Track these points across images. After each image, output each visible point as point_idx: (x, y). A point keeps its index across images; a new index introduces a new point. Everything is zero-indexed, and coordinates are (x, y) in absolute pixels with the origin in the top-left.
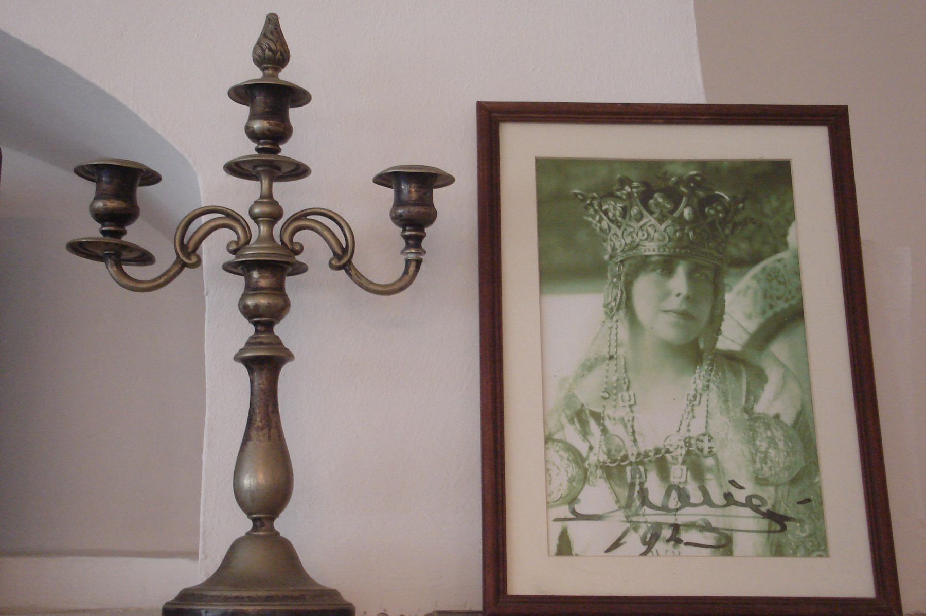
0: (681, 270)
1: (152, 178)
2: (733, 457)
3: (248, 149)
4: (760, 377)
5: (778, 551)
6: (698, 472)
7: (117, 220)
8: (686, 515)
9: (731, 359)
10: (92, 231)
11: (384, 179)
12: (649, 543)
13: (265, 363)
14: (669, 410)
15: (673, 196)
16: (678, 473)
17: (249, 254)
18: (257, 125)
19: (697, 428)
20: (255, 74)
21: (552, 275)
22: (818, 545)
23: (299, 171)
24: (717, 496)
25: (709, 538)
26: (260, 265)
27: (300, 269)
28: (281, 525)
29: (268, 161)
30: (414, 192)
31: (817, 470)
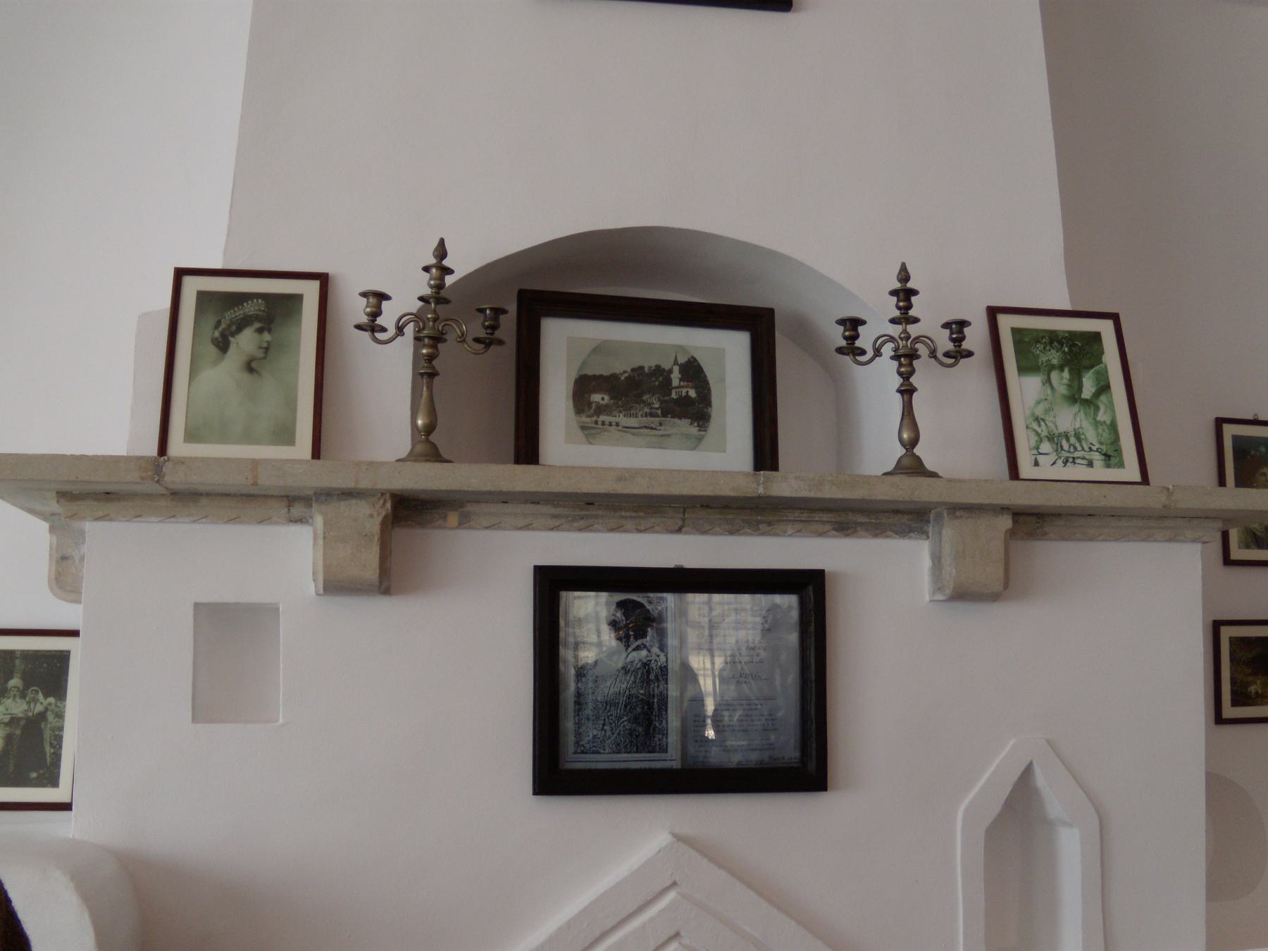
0: (1066, 370)
1: (863, 323)
2: (1091, 435)
3: (897, 313)
4: (1097, 408)
5: (1108, 466)
6: (1079, 440)
8: (1076, 454)
9: (1087, 402)
10: (843, 343)
11: (364, 295)
12: (1065, 463)
14: (1067, 419)
15: (1061, 343)
16: (1073, 440)
17: (901, 352)
18: (901, 304)
19: (1077, 426)
20: (898, 285)
21: (1023, 370)
22: (1121, 465)
23: (916, 320)
24: (1086, 448)
25: (1085, 462)
26: (905, 356)
27: (918, 357)
28: (918, 451)
29: (905, 318)
30: (957, 328)
31: (709, 404)
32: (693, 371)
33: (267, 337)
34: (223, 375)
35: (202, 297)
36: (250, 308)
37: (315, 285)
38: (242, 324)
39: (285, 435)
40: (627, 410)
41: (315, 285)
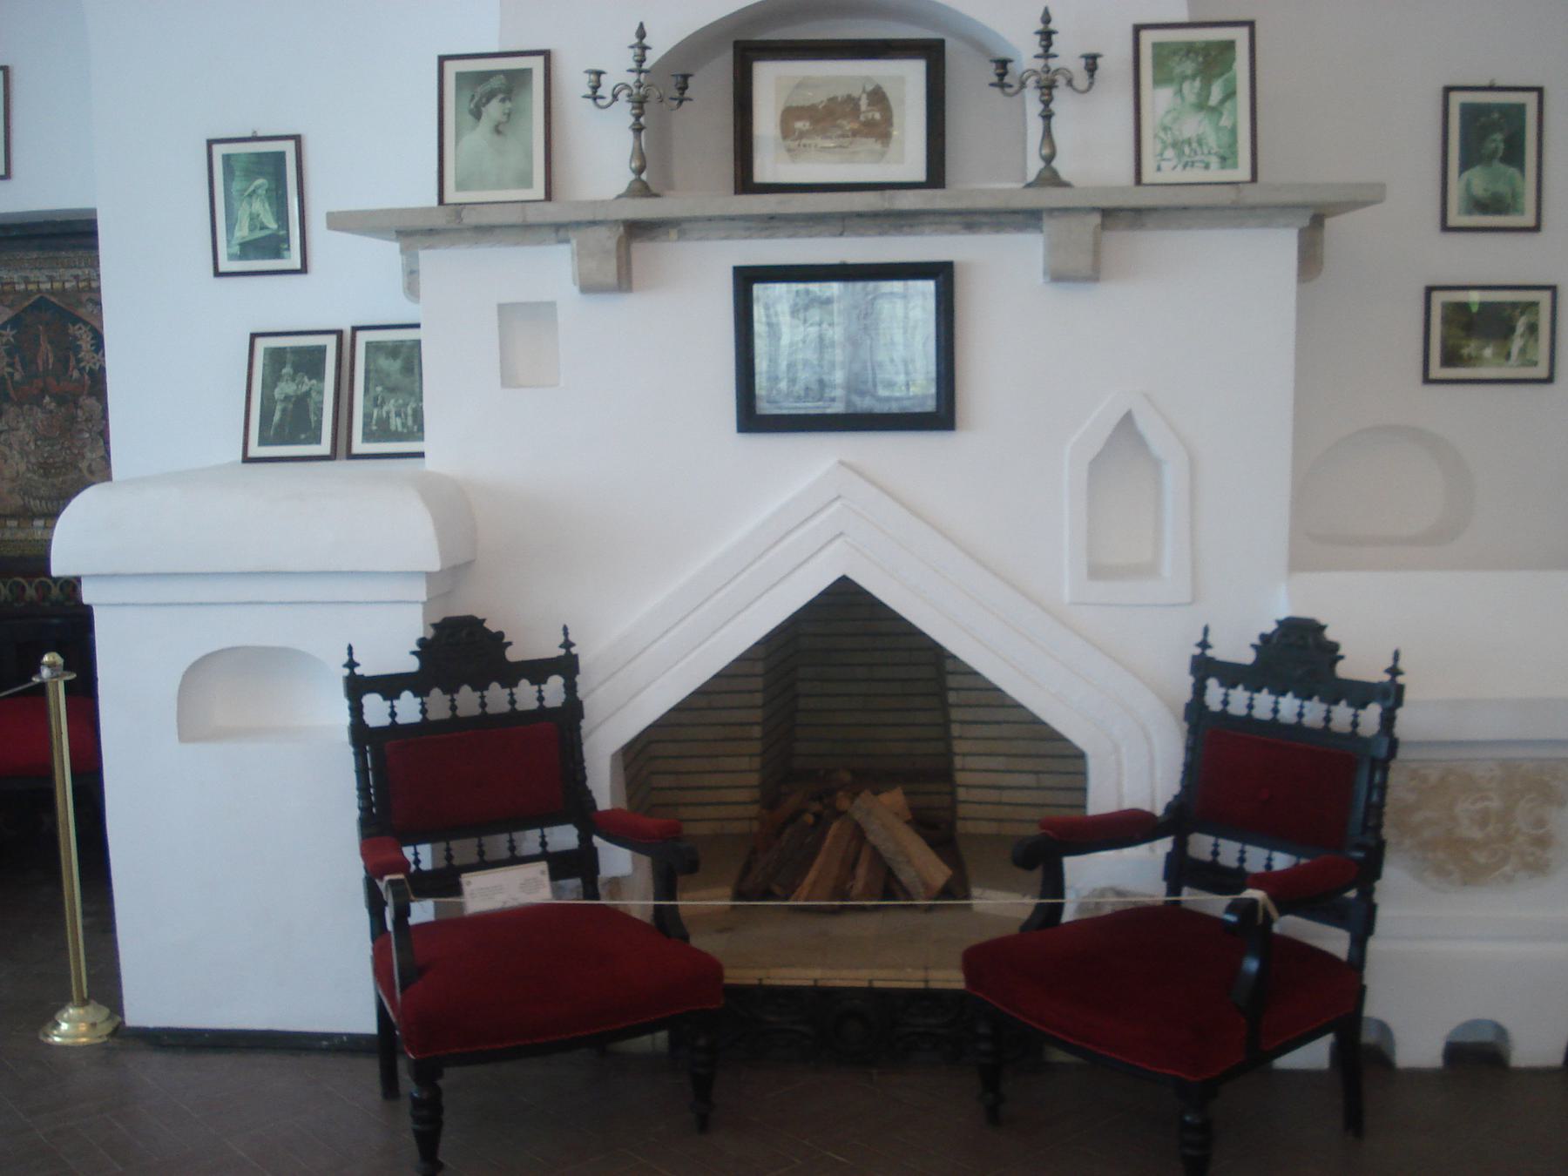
4: (1221, 114)
5: (1223, 168)
7: (1002, 76)
9: (1213, 110)
12: (1185, 166)
13: (1047, 116)
14: (1193, 126)
16: (1195, 145)
21: (1158, 82)
28: (1055, 164)
29: (1046, 54)
32: (878, 97)
33: (508, 105)
34: (479, 137)
35: (460, 76)
36: (495, 83)
37: (540, 60)
38: (490, 96)
39: (525, 181)
40: (824, 134)
41: (540, 60)
